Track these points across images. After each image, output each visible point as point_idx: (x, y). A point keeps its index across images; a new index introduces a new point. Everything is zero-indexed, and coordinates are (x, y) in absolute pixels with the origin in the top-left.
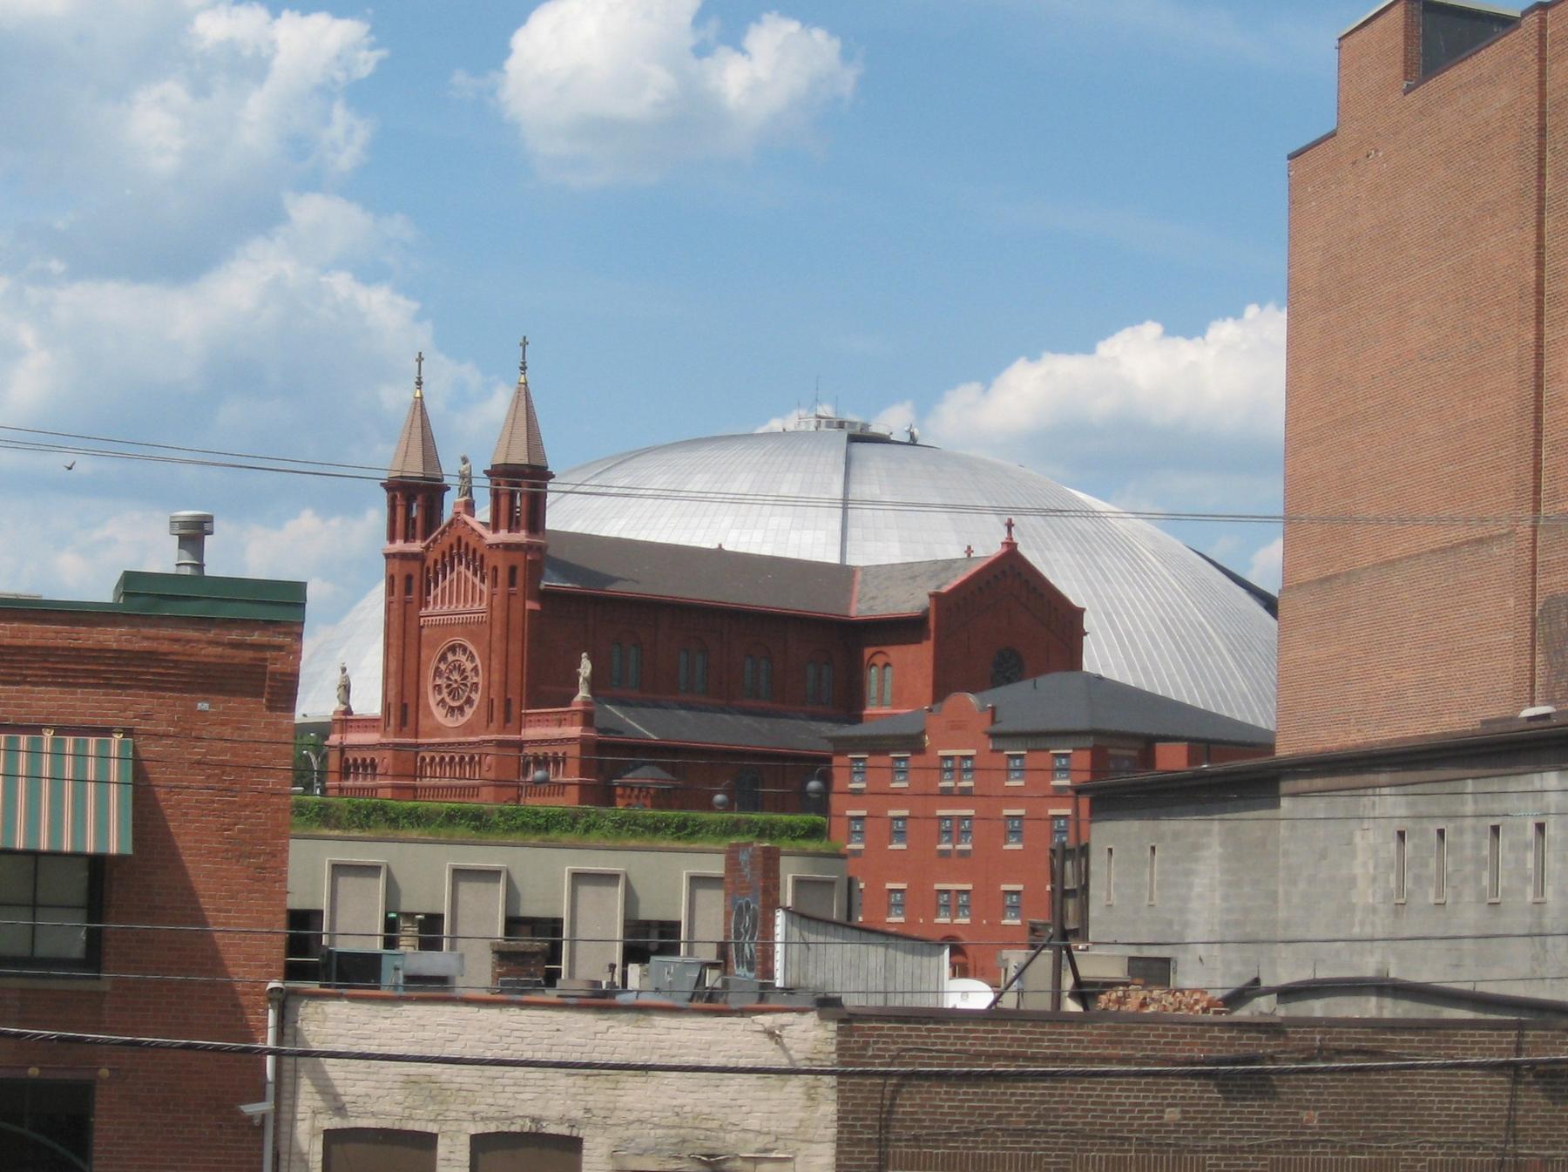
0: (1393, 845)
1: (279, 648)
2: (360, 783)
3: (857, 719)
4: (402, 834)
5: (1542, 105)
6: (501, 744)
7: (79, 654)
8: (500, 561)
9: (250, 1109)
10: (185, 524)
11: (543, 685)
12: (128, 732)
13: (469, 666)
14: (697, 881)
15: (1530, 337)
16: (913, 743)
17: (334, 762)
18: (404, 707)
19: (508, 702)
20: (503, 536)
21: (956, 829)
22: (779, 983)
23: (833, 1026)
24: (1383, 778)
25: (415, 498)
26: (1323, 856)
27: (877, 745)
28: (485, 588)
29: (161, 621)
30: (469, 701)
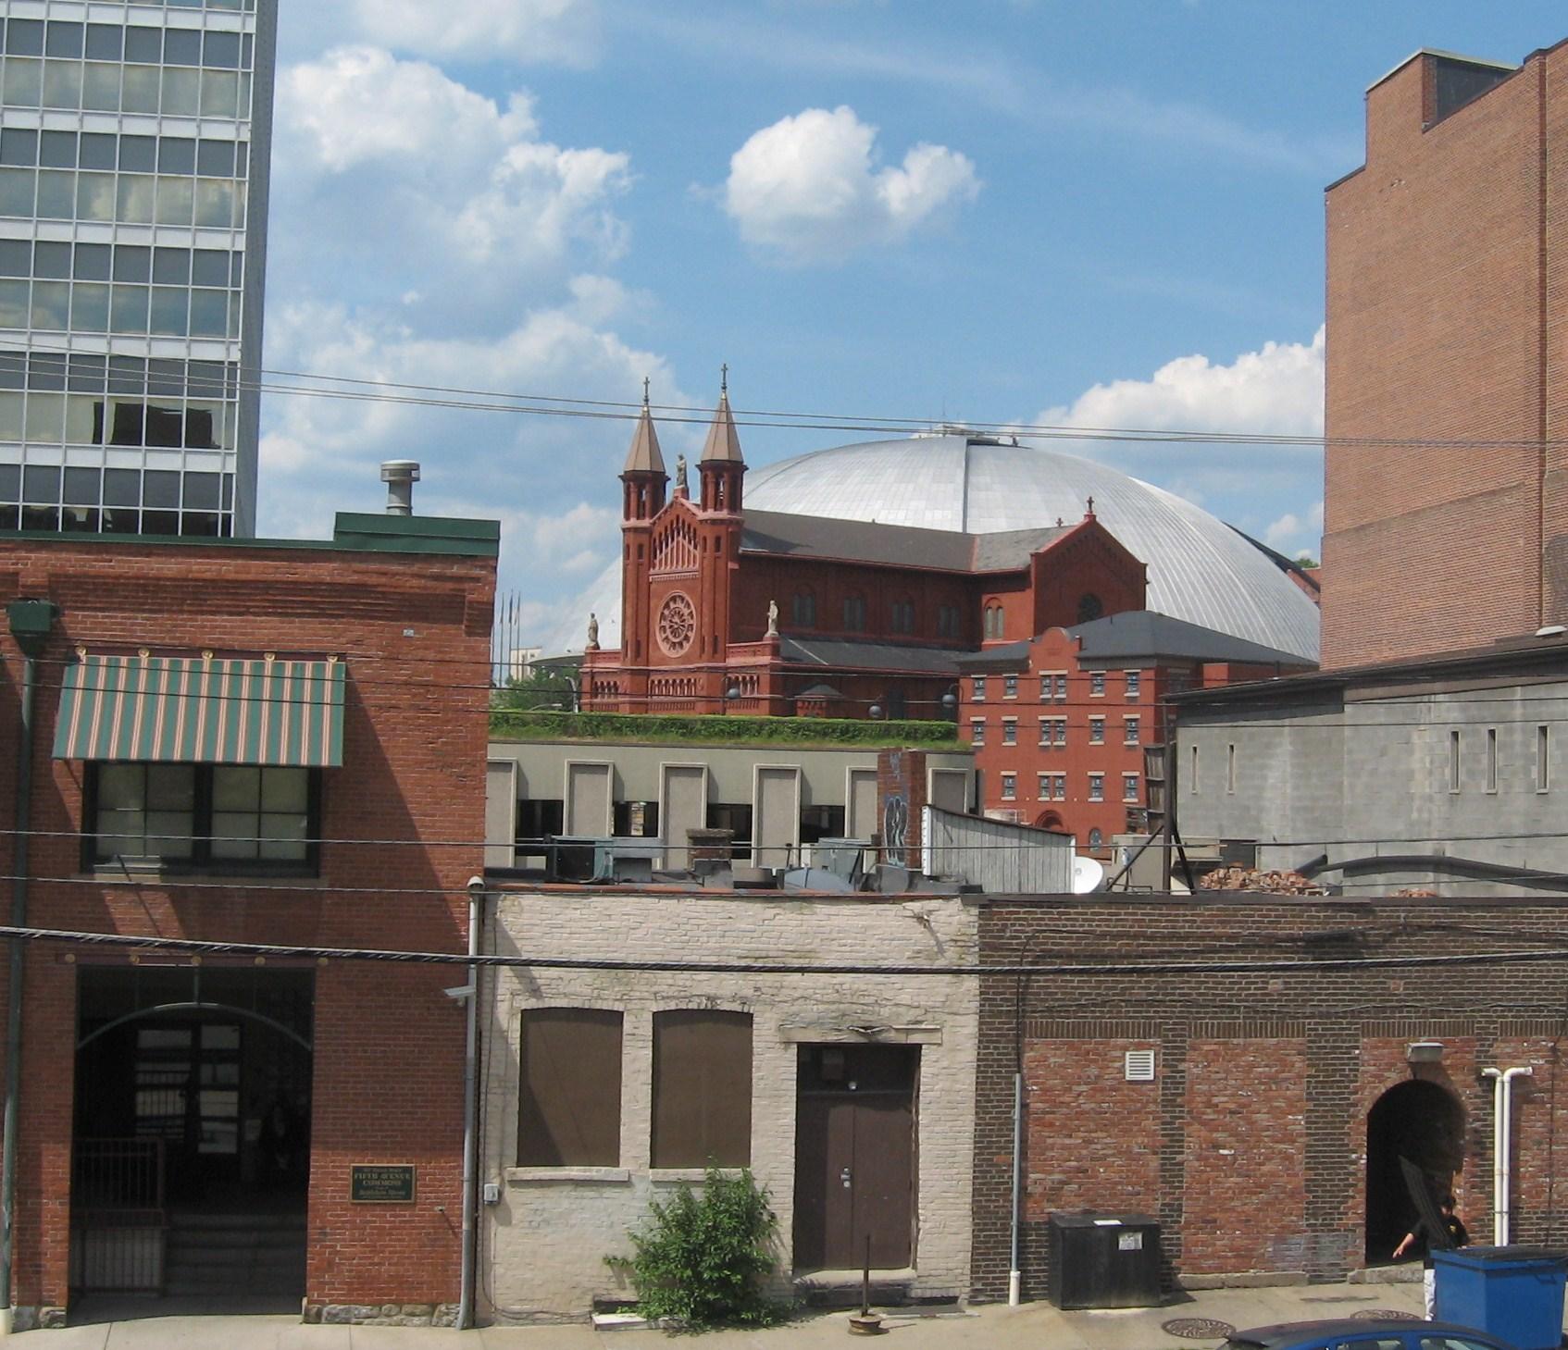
0: (1448, 743)
1: (477, 579)
2: (606, 700)
3: (978, 648)
4: (626, 740)
5: (1543, 133)
7: (295, 587)
8: (708, 532)
9: (453, 992)
10: (393, 472)
11: (743, 627)
12: (341, 657)
13: (686, 611)
14: (856, 774)
15: (1536, 324)
16: (1020, 666)
17: (586, 686)
18: (638, 644)
20: (710, 514)
21: (1054, 728)
22: (926, 872)
23: (975, 911)
24: (1438, 686)
25: (644, 487)
26: (1383, 753)
27: (993, 668)
28: (697, 553)
29: (368, 557)
30: (687, 638)
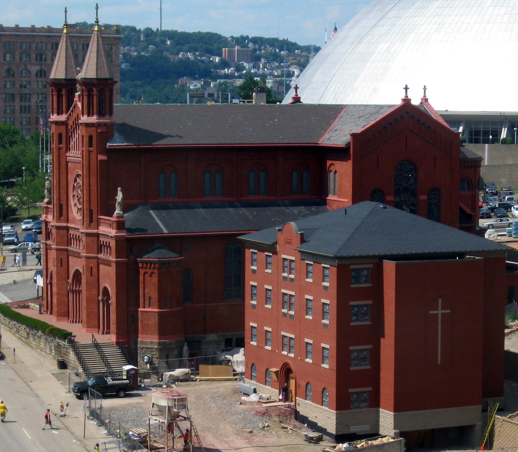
6: (87, 235)
19: (91, 212)
